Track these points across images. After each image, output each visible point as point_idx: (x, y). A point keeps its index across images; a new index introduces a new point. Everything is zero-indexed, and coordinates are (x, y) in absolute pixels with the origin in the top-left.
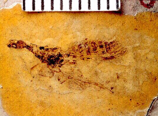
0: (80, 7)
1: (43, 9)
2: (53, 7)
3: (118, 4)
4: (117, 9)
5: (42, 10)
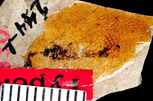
0: (76, 93)
1: (68, 91)
2: (59, 92)
4: (4, 85)
5: (69, 91)
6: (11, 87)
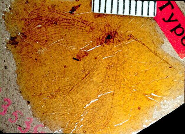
3: (155, 13)
5: (136, 14)
6: (148, 15)
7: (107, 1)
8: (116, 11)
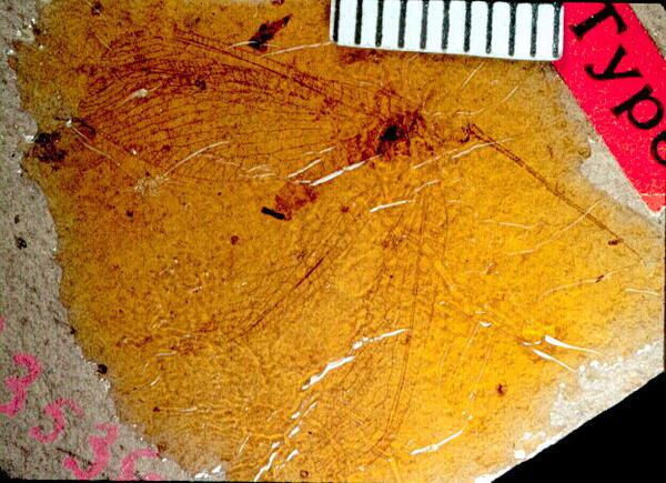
3: (557, 46)
5: (488, 52)
6: (533, 52)
7: (385, 4)
8: (418, 40)
